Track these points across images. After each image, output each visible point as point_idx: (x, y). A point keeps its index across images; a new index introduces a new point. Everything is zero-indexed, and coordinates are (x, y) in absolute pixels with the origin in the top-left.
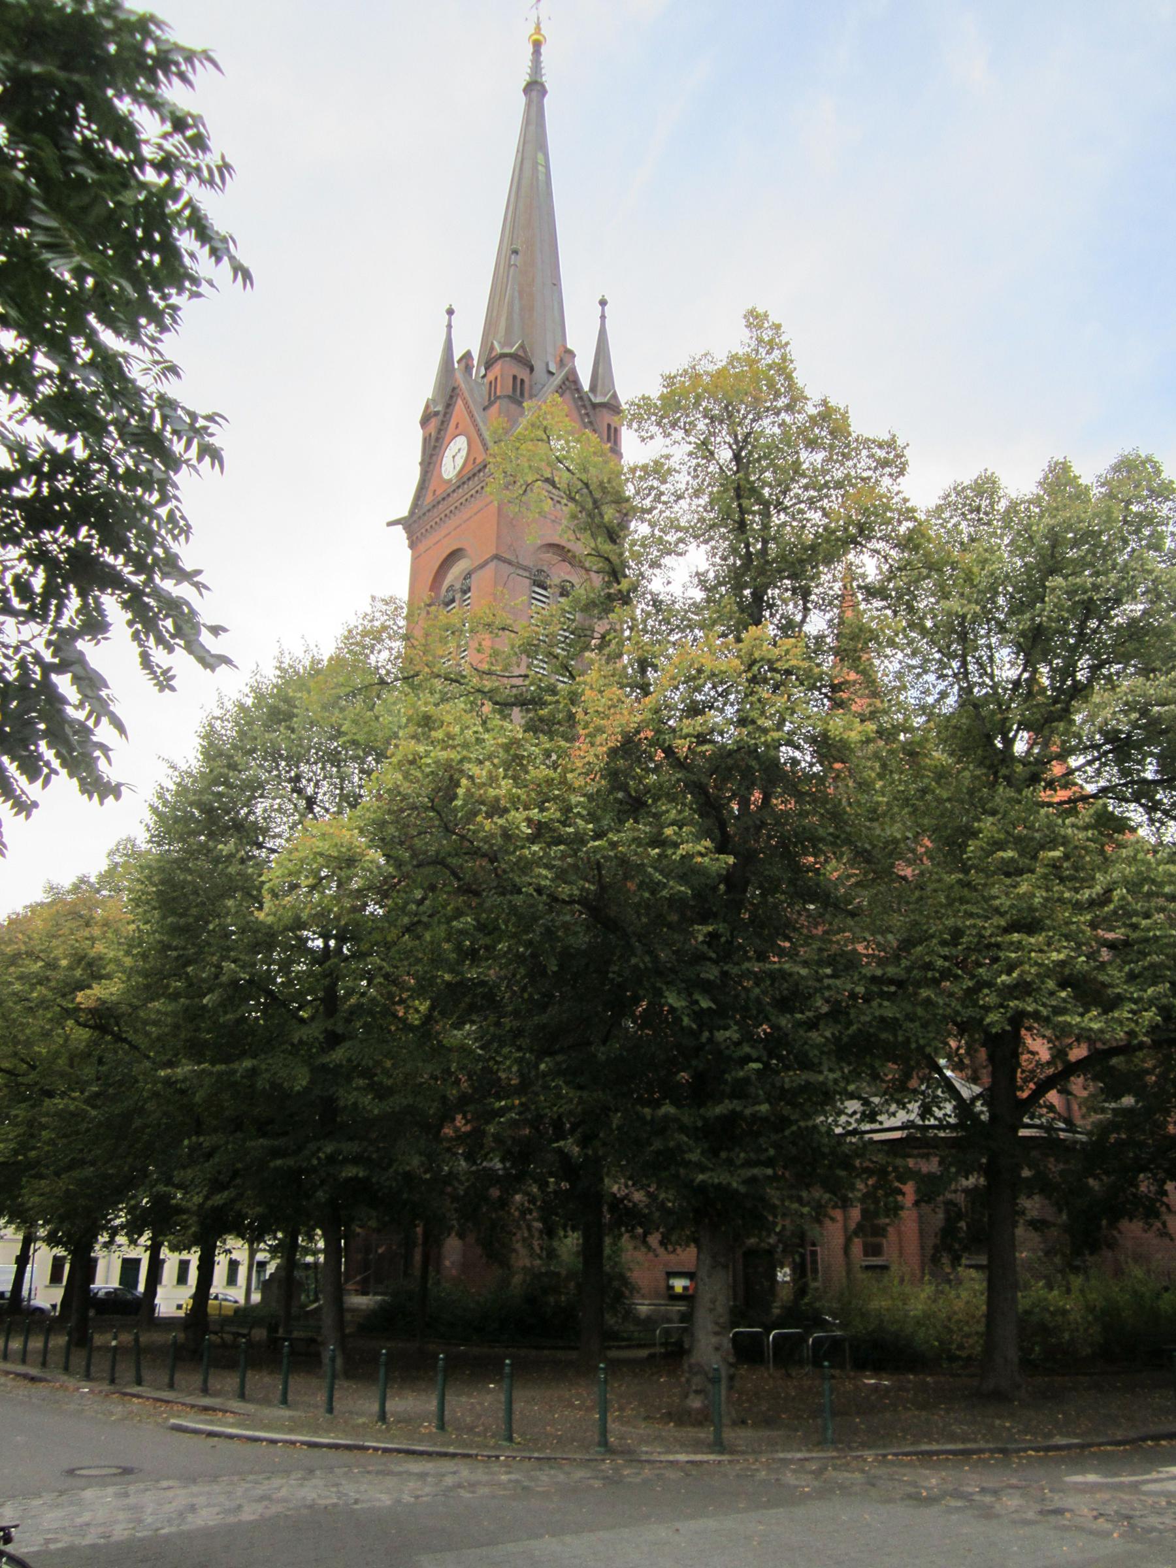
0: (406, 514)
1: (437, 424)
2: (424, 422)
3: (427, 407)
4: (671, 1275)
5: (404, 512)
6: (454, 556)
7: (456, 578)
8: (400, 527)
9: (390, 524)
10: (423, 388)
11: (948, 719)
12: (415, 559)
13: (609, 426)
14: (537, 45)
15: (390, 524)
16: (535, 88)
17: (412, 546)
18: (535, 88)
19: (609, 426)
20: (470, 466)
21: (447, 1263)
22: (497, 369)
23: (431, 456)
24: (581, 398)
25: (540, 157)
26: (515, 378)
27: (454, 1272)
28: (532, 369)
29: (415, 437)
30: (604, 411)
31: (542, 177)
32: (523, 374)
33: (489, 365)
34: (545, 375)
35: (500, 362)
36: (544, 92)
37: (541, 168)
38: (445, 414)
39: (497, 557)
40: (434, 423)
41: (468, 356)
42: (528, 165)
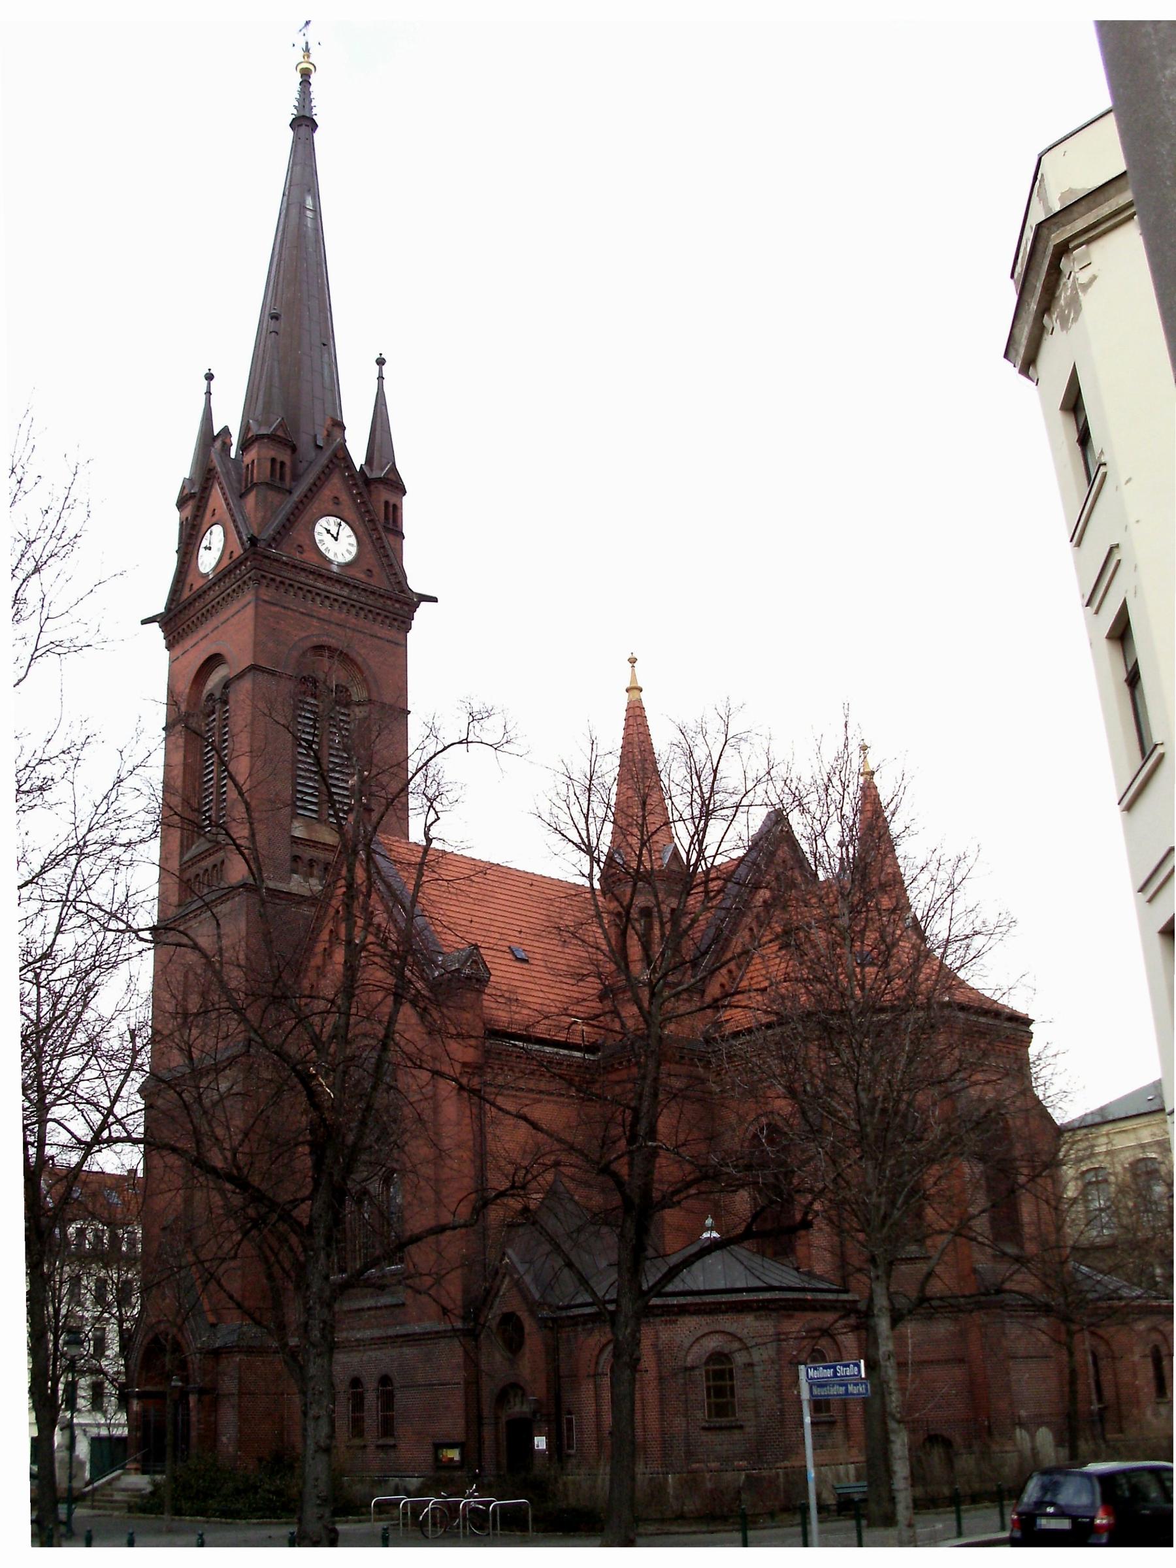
0: (162, 610)
1: (195, 504)
2: (181, 504)
3: (183, 488)
4: (438, 1447)
5: (159, 607)
6: (214, 661)
7: (216, 686)
8: (156, 624)
9: (144, 622)
10: (179, 464)
11: (682, 877)
12: (173, 661)
13: (387, 503)
14: (306, 75)
15: (144, 622)
16: (304, 123)
17: (169, 647)
18: (304, 123)
19: (387, 503)
20: (226, 562)
21: (224, 1439)
22: (252, 454)
23: (188, 544)
24: (351, 476)
25: (309, 203)
26: (273, 460)
27: (231, 1449)
28: (294, 449)
29: (171, 521)
30: (381, 487)
31: (309, 223)
32: (284, 456)
33: (244, 446)
34: (312, 453)
35: (256, 444)
36: (314, 126)
37: (309, 214)
38: (202, 498)
39: (254, 668)
40: (189, 510)
41: (226, 431)
42: (294, 211)
